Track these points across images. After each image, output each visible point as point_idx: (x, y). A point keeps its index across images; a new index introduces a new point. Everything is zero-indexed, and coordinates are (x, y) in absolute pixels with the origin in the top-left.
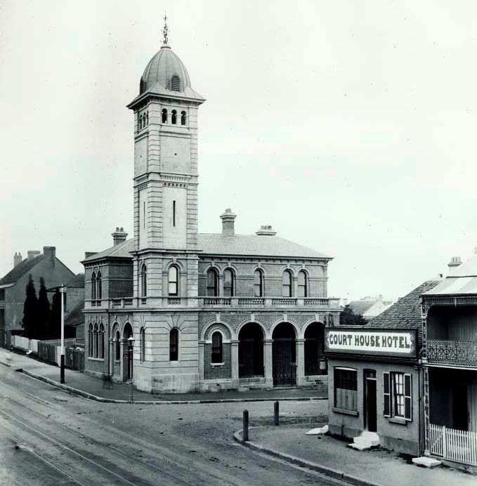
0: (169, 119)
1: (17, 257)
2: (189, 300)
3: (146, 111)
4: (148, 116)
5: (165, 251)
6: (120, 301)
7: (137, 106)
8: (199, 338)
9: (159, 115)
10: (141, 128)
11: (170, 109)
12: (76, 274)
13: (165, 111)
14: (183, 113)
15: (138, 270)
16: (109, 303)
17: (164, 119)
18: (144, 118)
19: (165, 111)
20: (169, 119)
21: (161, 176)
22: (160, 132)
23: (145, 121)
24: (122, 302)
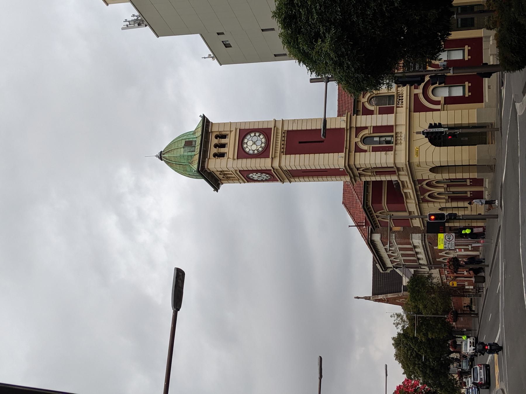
0: (222, 150)
1: (393, 338)
2: (415, 160)
3: (218, 174)
4: (221, 171)
5: (408, 110)
6: (405, 193)
7: (215, 181)
8: (439, 110)
9: (218, 160)
10: (234, 177)
11: (214, 150)
12: (405, 377)
13: (215, 155)
14: (217, 137)
15: (370, 176)
16: (410, 203)
17: (222, 155)
18: (225, 174)
19: (215, 155)
20: (222, 150)
21: (275, 157)
22: (234, 159)
23: (227, 174)
24: (405, 191)
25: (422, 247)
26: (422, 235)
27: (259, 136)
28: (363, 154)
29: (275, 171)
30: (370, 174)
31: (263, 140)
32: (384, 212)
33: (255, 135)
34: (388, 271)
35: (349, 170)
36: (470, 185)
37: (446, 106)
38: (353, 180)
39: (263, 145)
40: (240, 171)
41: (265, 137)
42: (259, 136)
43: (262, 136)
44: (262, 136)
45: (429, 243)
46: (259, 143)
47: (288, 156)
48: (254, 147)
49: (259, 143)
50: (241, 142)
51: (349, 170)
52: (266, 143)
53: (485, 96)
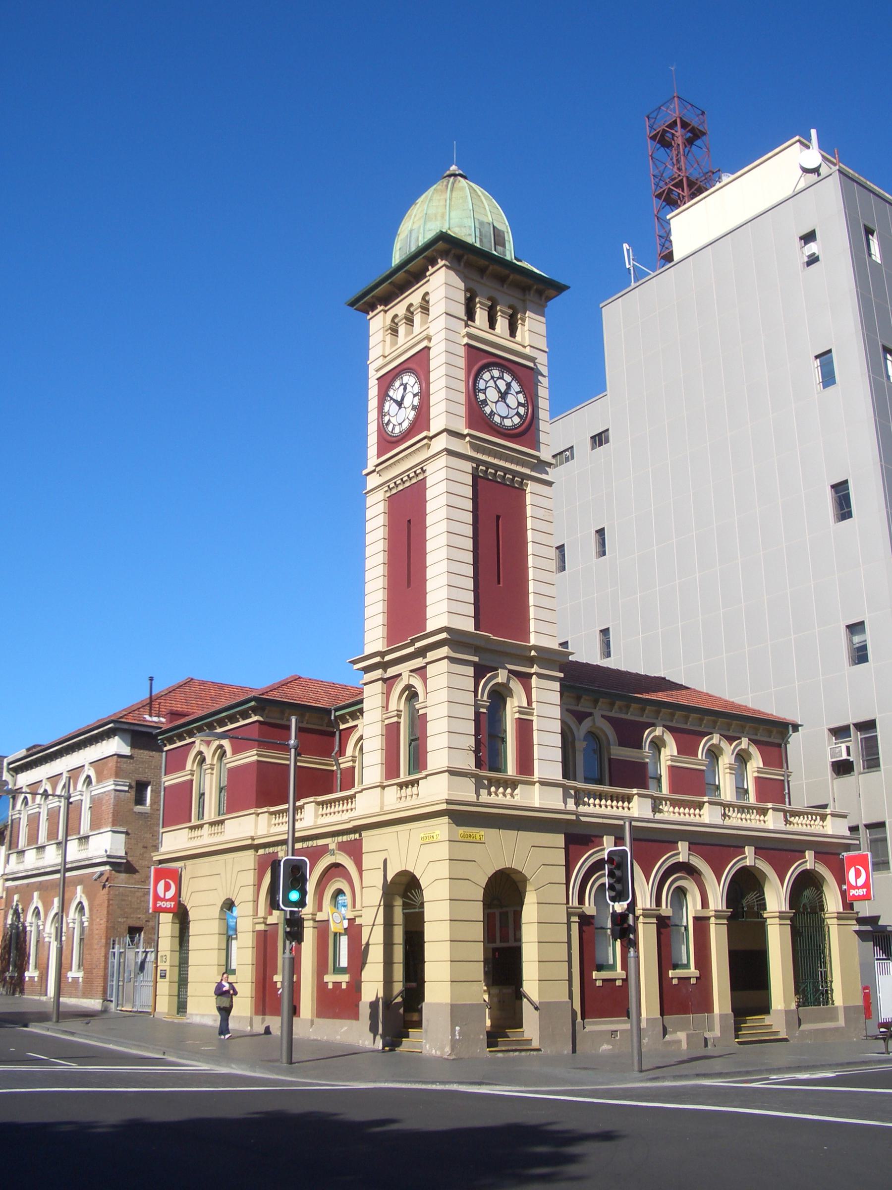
25: (83, 855)
26: (120, 857)
27: (518, 414)
28: (470, 684)
29: (426, 441)
30: (393, 706)
31: (508, 423)
32: (27, 804)
33: (520, 404)
34: (6, 776)
35: (418, 645)
36: (321, 986)
37: (655, 920)
38: (377, 659)
39: (497, 419)
40: (427, 348)
41: (515, 427)
42: (518, 414)
43: (516, 420)
44: (516, 420)
45: (102, 874)
46: (501, 409)
47: (469, 480)
48: (492, 395)
49: (501, 409)
50: (504, 365)
51: (418, 645)
52: (502, 426)
53: (612, 1023)
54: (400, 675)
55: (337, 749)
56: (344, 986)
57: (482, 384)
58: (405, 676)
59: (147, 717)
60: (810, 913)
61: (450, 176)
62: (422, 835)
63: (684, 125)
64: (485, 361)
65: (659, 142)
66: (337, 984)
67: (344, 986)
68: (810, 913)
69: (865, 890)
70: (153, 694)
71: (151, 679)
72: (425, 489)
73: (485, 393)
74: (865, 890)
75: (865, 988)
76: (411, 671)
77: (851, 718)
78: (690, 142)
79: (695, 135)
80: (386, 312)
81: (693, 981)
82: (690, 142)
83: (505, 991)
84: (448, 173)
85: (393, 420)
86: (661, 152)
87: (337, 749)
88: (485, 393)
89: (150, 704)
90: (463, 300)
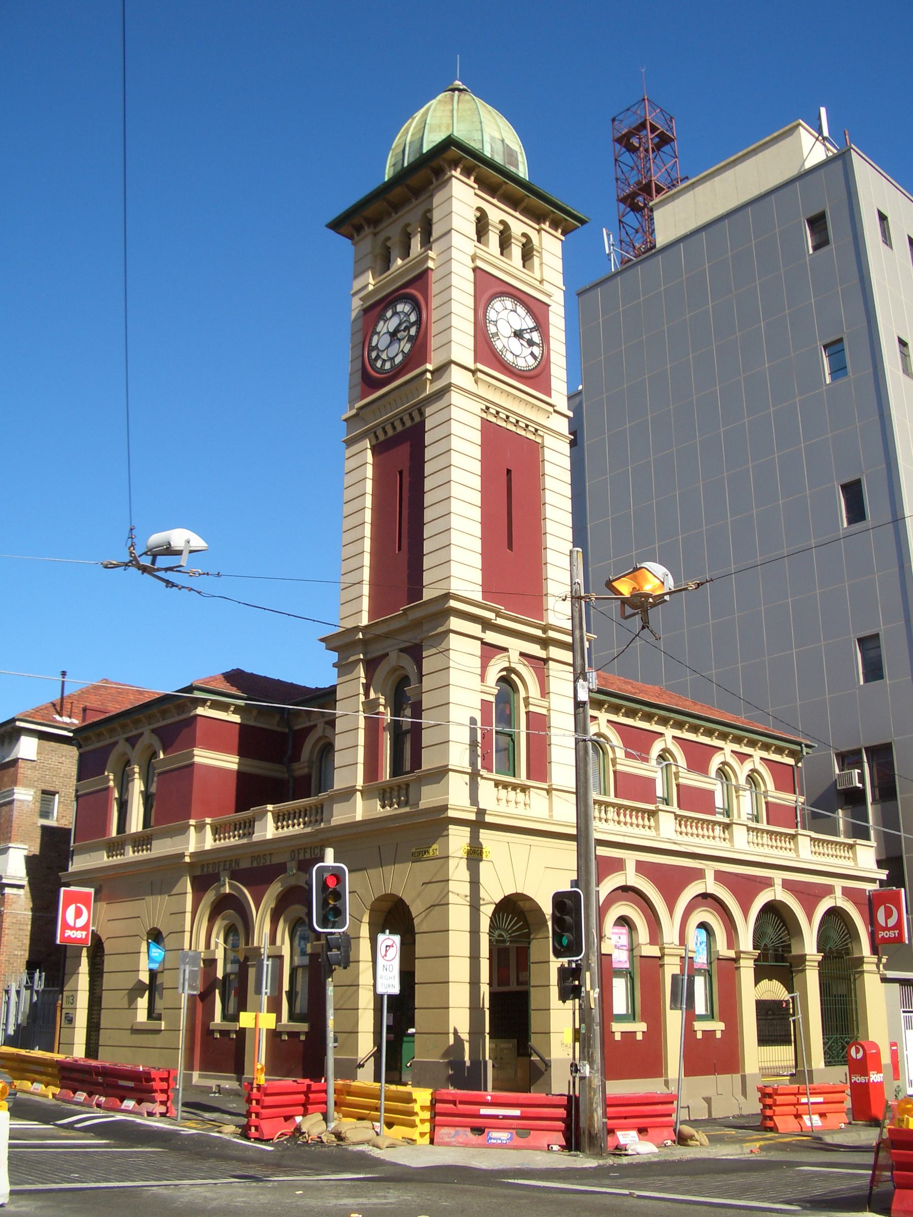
43: (531, 362)
44: (531, 362)
54: (387, 654)
55: (290, 753)
56: (639, 1037)
57: (492, 315)
58: (393, 656)
59: (58, 717)
60: (836, 957)
61: (453, 90)
62: (413, 850)
63: (654, 129)
64: (498, 289)
65: (625, 147)
66: (709, 1034)
67: (639, 1037)
68: (836, 957)
69: (897, 932)
70: (66, 693)
71: (64, 674)
72: (423, 432)
73: (496, 325)
74: (897, 932)
75: (893, 1044)
76: (401, 650)
77: (865, 740)
78: (658, 147)
79: (664, 140)
80: (375, 235)
81: (303, 1038)
82: (658, 147)
83: (503, 1046)
84: (451, 87)
85: (384, 356)
86: (627, 157)
87: (290, 753)
88: (496, 325)
89: (59, 707)
90: (474, 219)
